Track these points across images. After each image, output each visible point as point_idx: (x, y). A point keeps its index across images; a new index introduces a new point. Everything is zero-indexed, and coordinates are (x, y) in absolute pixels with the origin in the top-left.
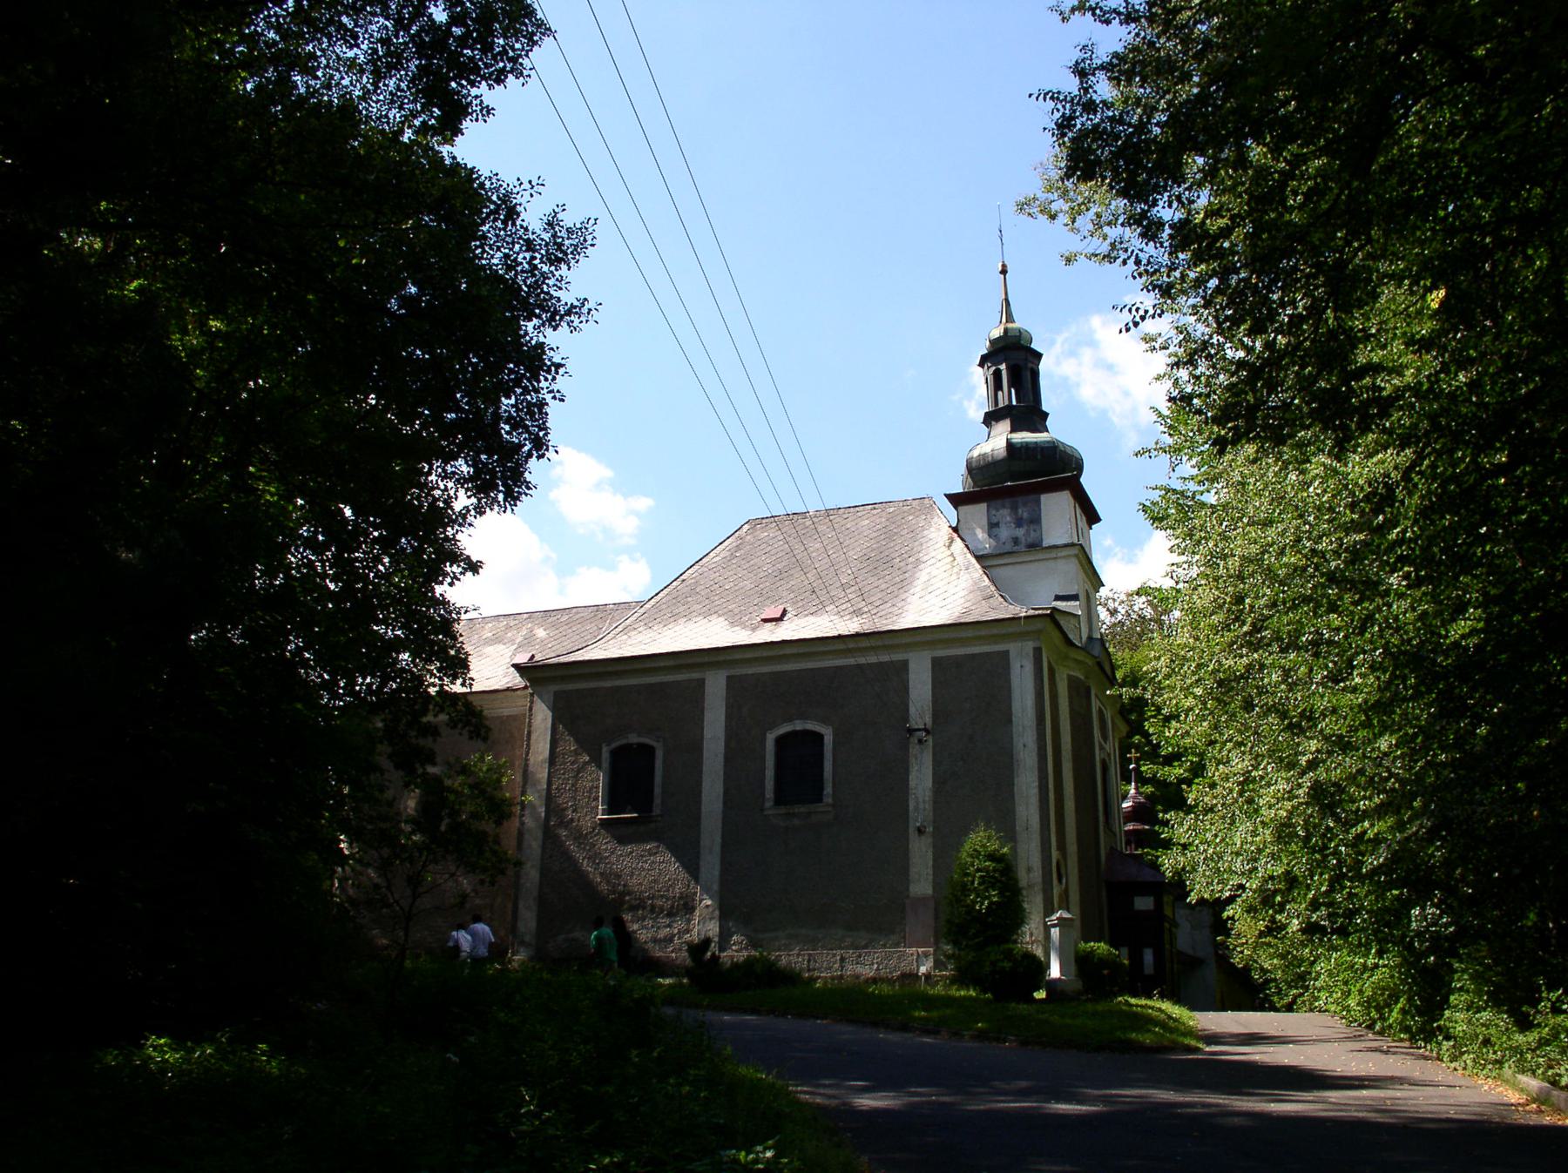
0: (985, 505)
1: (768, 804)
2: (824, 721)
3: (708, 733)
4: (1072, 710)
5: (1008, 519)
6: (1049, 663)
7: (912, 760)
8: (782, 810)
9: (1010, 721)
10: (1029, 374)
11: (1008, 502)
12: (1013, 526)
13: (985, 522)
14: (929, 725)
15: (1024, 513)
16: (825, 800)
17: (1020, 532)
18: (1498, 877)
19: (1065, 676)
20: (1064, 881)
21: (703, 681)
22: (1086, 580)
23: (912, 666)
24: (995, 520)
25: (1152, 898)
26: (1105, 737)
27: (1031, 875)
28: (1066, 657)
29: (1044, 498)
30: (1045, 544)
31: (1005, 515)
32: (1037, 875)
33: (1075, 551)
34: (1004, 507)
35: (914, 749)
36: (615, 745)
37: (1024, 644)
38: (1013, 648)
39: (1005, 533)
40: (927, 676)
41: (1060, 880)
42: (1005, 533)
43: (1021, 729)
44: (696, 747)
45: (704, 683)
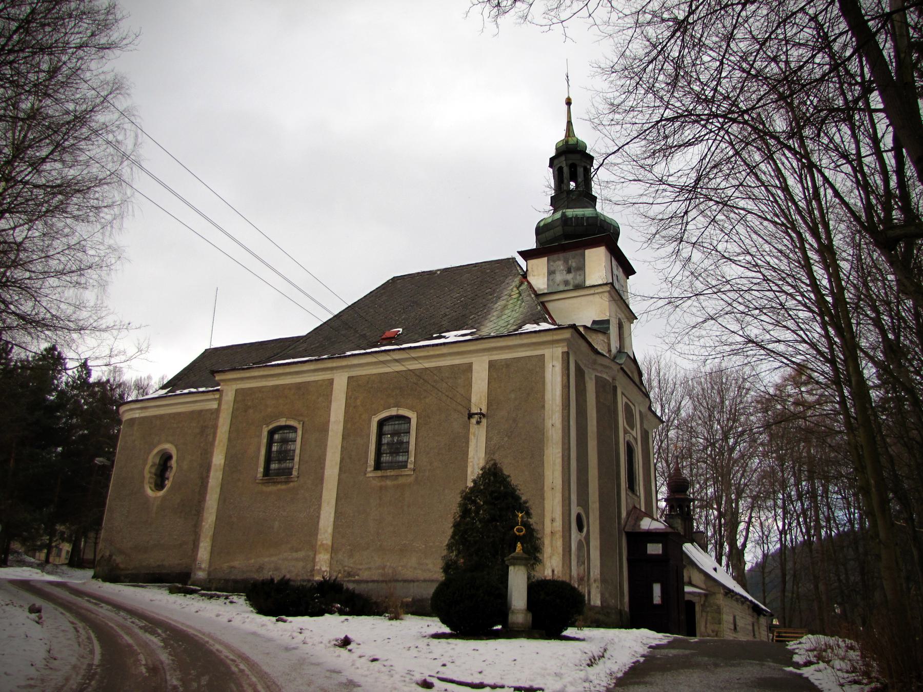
0: (546, 259)
1: (369, 469)
2: (411, 408)
3: (333, 418)
4: (598, 402)
5: (562, 268)
6: (576, 363)
7: (471, 437)
8: (379, 473)
9: (543, 407)
10: (582, 170)
11: (561, 255)
12: (565, 272)
13: (545, 271)
14: (484, 411)
15: (573, 263)
16: (409, 466)
17: (569, 277)
18: (63, 452)
19: (593, 377)
20: (585, 530)
21: (332, 380)
22: (618, 310)
23: (475, 367)
24: (552, 269)
25: (648, 545)
26: (632, 425)
27: (554, 524)
28: (595, 362)
29: (587, 252)
30: (588, 283)
31: (560, 265)
32: (558, 525)
33: (607, 288)
34: (559, 260)
35: (473, 428)
36: (271, 427)
37: (555, 349)
38: (547, 352)
39: (559, 277)
40: (485, 375)
41: (580, 528)
42: (559, 277)
43: (550, 412)
44: (324, 429)
45: (333, 382)
